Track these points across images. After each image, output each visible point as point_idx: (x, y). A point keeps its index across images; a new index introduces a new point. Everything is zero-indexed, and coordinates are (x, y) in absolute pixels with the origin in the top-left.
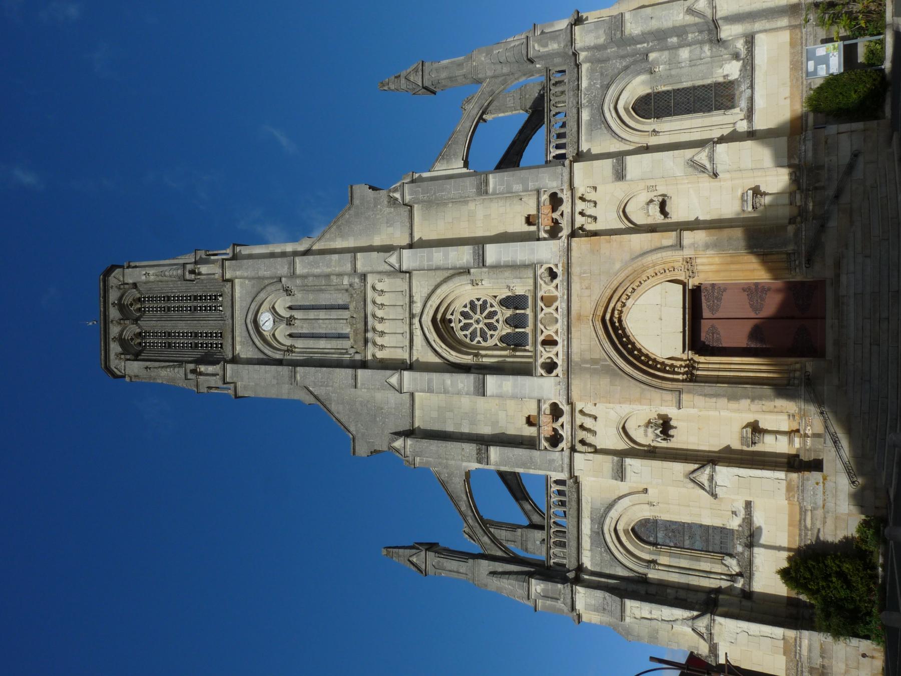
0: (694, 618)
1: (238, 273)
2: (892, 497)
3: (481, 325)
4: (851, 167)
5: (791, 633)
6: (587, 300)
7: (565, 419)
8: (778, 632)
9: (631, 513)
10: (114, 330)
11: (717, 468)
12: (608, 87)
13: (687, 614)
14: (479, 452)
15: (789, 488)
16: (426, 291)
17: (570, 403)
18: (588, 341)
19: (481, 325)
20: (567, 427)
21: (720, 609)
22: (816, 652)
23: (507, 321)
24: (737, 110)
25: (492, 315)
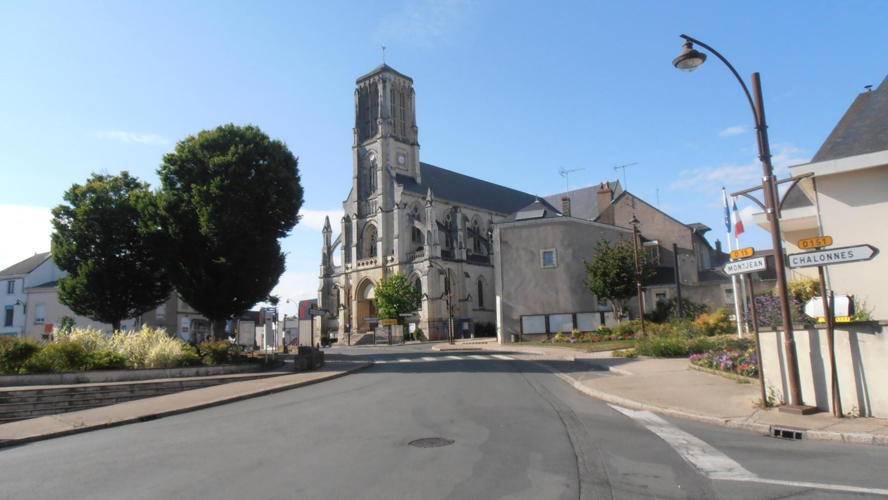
10: (367, 82)
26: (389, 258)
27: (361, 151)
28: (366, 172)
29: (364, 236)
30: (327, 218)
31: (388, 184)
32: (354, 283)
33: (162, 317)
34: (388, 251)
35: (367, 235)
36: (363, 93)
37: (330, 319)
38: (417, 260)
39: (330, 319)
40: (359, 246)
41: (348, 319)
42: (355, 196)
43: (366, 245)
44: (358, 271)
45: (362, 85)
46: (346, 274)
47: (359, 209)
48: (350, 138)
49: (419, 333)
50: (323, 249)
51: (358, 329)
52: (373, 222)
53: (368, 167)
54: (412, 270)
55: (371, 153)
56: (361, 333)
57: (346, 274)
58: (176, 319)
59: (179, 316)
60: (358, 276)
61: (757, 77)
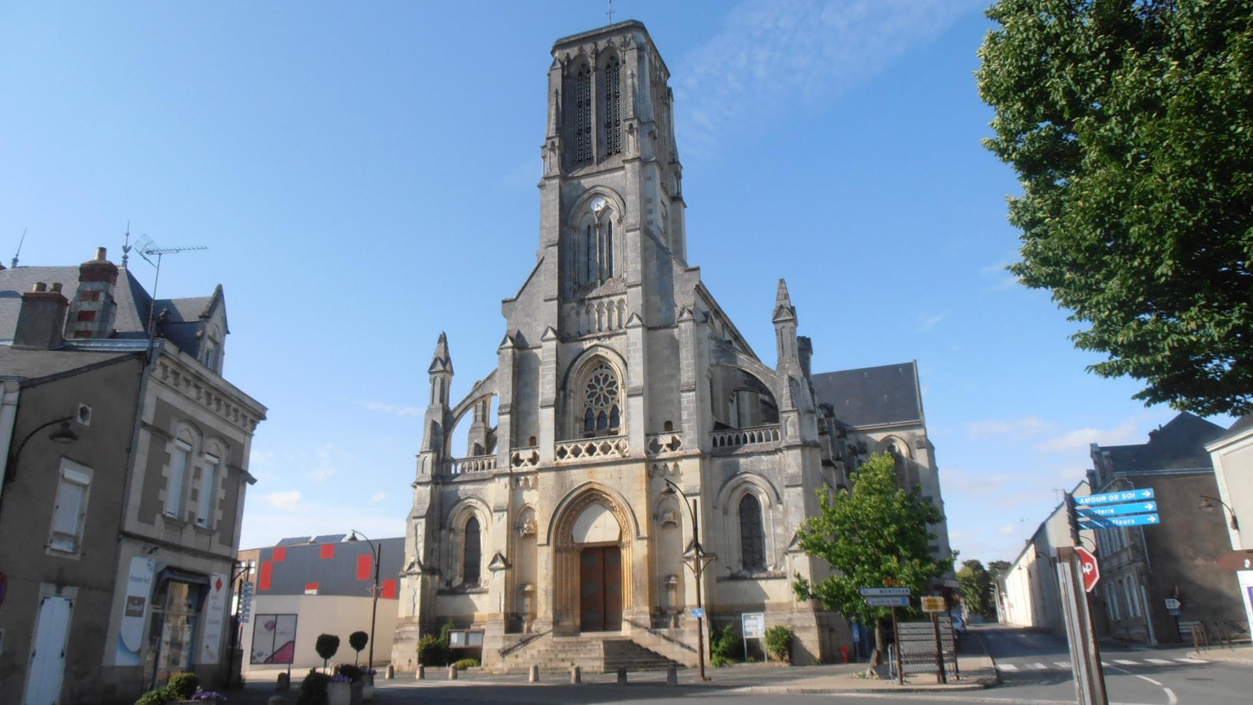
0: (419, 562)
1: (629, 175)
2: (765, 689)
3: (605, 389)
4: (682, 645)
5: (417, 619)
6: (603, 478)
7: (530, 467)
8: (417, 613)
9: (482, 516)
10: (588, 48)
11: (646, 542)
12: (761, 475)
13: (421, 559)
14: (505, 406)
15: (495, 615)
16: (617, 348)
17: (540, 470)
18: (579, 478)
19: (605, 389)
20: (525, 469)
21: (429, 578)
22: (408, 635)
23: (602, 412)
24: (741, 567)
25: (606, 399)
26: (665, 440)
27: (566, 189)
28: (579, 237)
29: (571, 385)
30: (443, 339)
31: (653, 264)
32: (541, 502)
33: (66, 546)
34: (660, 423)
35: (577, 382)
36: (574, 70)
37: (441, 592)
38: (749, 447)
39: (441, 592)
40: (560, 407)
41: (518, 592)
42: (549, 284)
43: (576, 406)
44: (558, 469)
45: (573, 52)
46: (515, 477)
47: (561, 319)
48: (531, 164)
49: (787, 644)
50: (430, 411)
51: (556, 623)
52: (602, 352)
53: (584, 227)
54: (733, 472)
55: (598, 195)
56: (564, 634)
57: (515, 477)
58: (116, 556)
59: (126, 548)
60: (561, 483)
61: (785, 314)
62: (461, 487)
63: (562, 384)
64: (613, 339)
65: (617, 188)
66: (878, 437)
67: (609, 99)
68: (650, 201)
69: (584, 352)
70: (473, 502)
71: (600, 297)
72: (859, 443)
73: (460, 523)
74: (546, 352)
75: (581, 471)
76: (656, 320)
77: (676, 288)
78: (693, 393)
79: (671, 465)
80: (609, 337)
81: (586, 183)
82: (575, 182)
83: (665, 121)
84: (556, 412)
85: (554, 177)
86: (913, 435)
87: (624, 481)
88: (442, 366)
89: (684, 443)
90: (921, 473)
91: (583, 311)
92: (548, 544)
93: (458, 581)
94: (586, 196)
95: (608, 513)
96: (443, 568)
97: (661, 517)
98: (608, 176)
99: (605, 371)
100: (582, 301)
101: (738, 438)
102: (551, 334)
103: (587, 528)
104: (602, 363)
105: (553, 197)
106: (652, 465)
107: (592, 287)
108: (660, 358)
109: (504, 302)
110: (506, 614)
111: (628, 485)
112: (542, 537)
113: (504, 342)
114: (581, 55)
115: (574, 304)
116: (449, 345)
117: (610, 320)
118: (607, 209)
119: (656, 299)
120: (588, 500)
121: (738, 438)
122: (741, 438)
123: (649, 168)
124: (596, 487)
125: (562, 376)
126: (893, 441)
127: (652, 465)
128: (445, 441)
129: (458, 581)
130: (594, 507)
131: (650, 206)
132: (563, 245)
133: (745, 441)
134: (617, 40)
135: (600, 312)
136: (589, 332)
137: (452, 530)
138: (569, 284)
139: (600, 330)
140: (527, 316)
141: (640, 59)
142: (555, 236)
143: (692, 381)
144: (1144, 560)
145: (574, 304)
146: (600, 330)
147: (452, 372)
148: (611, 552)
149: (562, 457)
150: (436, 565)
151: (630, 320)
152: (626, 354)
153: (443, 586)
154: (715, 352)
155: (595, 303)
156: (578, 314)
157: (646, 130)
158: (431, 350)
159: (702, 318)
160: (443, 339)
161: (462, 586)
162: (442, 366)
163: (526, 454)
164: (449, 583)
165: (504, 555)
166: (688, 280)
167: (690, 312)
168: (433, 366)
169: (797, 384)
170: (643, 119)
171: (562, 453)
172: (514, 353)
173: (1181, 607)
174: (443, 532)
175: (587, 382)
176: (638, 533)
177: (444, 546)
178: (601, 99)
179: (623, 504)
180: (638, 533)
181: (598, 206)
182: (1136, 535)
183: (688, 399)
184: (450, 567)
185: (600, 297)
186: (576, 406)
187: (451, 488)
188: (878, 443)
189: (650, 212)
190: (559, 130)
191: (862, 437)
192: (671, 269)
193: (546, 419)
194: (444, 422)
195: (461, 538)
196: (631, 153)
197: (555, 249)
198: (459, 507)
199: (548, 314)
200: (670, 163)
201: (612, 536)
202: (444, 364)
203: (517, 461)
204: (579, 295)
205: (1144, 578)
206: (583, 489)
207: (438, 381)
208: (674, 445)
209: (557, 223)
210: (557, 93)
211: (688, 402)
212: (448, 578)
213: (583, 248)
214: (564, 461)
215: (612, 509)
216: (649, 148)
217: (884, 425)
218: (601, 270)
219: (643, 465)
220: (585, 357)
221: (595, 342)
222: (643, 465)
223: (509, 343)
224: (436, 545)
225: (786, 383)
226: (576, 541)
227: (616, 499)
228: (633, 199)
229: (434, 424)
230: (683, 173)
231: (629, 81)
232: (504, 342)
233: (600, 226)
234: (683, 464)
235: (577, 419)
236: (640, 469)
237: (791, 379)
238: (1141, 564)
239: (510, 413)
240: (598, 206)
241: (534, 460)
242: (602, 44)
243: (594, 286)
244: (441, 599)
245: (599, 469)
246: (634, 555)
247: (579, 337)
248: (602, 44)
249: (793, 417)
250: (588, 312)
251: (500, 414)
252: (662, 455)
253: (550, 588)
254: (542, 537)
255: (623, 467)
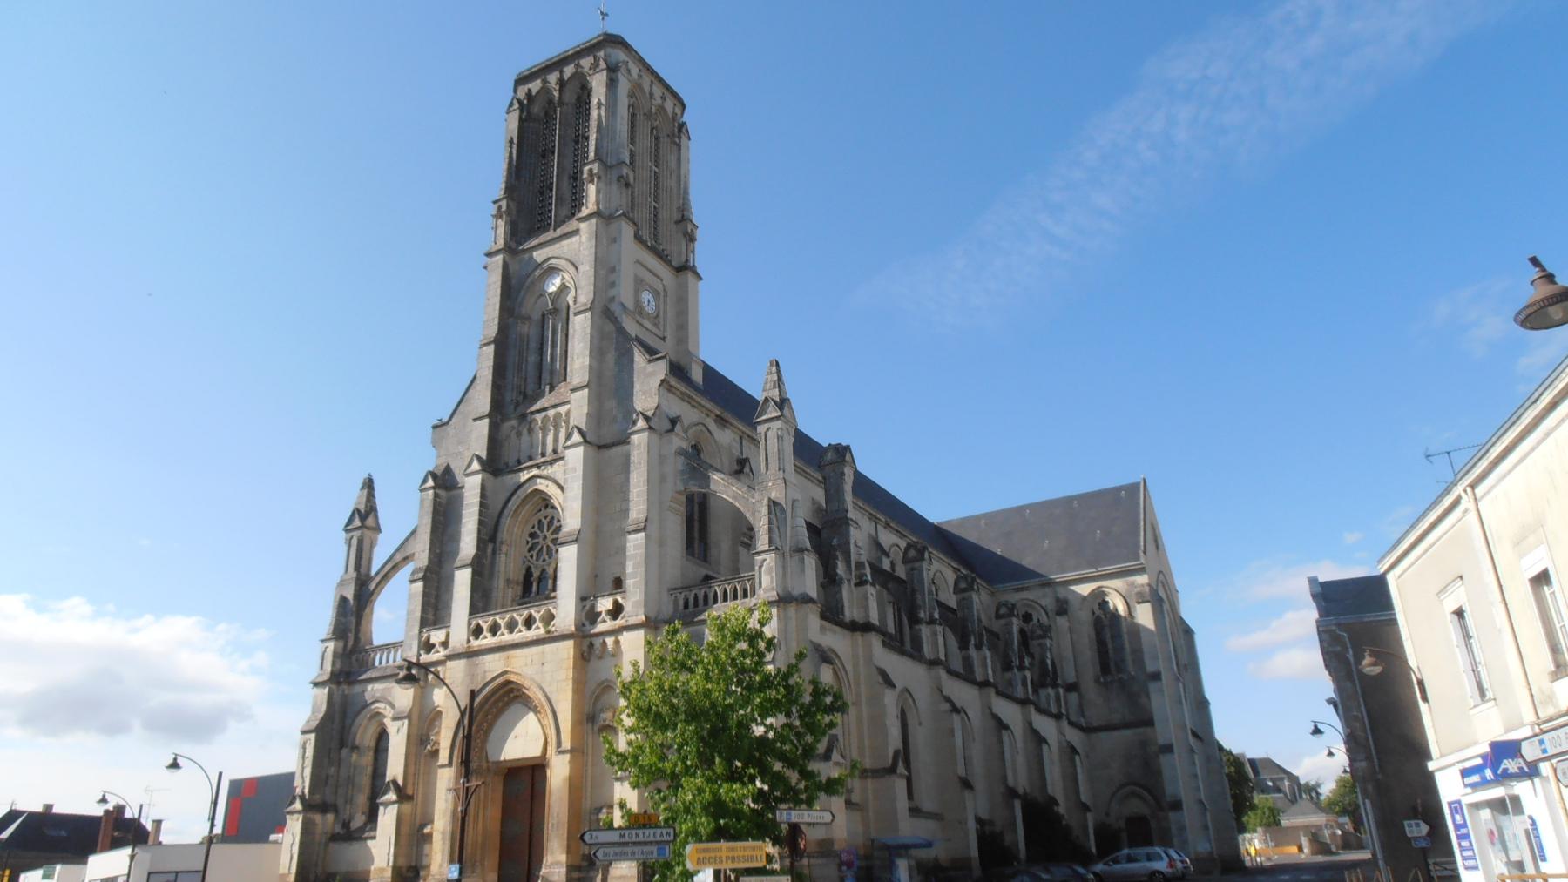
6: (526, 666)
10: (553, 78)
11: (567, 757)
18: (493, 665)
27: (513, 268)
28: (527, 330)
29: (503, 535)
30: (369, 485)
31: (611, 357)
34: (602, 578)
35: (514, 531)
36: (536, 109)
37: (335, 838)
39: (335, 838)
40: (482, 569)
42: (482, 400)
43: (509, 565)
44: (470, 654)
45: (535, 86)
47: (494, 442)
50: (342, 584)
52: (542, 485)
53: (536, 316)
55: (553, 270)
62: (370, 687)
63: (489, 535)
64: (556, 466)
65: (572, 259)
66: (1084, 589)
67: (577, 142)
68: (613, 270)
69: (520, 486)
70: (380, 706)
71: (545, 409)
72: (1058, 600)
73: (366, 737)
74: (472, 485)
75: (497, 656)
76: (608, 434)
77: (637, 387)
78: (642, 534)
79: (610, 641)
80: (551, 463)
81: (539, 255)
82: (526, 256)
83: (673, 165)
84: (474, 574)
85: (497, 252)
86: (1132, 585)
87: (547, 667)
88: (365, 518)
89: (628, 608)
90: (1145, 639)
91: (525, 431)
92: (450, 764)
93: (358, 821)
94: (537, 273)
95: (531, 715)
96: (340, 802)
97: (592, 717)
98: (565, 243)
99: (549, 510)
100: (523, 417)
101: (706, 596)
102: (476, 466)
103: (504, 740)
104: (545, 502)
105: (495, 279)
106: (586, 642)
107: (539, 395)
108: (604, 490)
109: (435, 427)
110: (394, 868)
111: (548, 671)
112: (443, 757)
113: (425, 481)
114: (545, 89)
115: (514, 422)
116: (377, 493)
117: (556, 440)
118: (563, 288)
119: (611, 404)
120: (506, 698)
121: (706, 596)
122: (711, 596)
123: (614, 226)
124: (513, 678)
125: (491, 523)
126: (1104, 594)
127: (586, 642)
128: (358, 624)
129: (358, 821)
130: (516, 708)
131: (612, 277)
132: (503, 343)
133: (715, 602)
134: (586, 62)
135: (544, 429)
136: (531, 459)
137: (355, 748)
138: (510, 396)
139: (543, 455)
140: (460, 443)
141: (612, 84)
142: (493, 330)
143: (643, 517)
144: (1369, 758)
145: (514, 422)
146: (543, 455)
147: (378, 529)
148: (534, 771)
149: (477, 638)
150: (330, 799)
151: (569, 436)
152: (565, 483)
153: (338, 829)
154: (683, 472)
155: (539, 417)
156: (519, 434)
157: (614, 174)
158: (353, 498)
159: (668, 426)
160: (369, 485)
161: (362, 829)
162: (365, 518)
163: (437, 636)
164: (346, 825)
165: (400, 782)
166: (652, 374)
167: (647, 419)
168: (350, 521)
169: (783, 511)
170: (611, 161)
171: (477, 632)
172: (436, 495)
173: (1429, 834)
174: (345, 751)
175: (528, 530)
176: (559, 744)
177: (343, 772)
178: (578, 145)
179: (545, 703)
180: (559, 744)
181: (553, 286)
182: (1356, 718)
183: (635, 544)
184: (349, 800)
185: (545, 409)
186: (509, 565)
187: (357, 688)
188: (1084, 598)
189: (613, 285)
190: (510, 190)
191: (1061, 592)
192: (632, 361)
193: (462, 580)
194: (357, 596)
195: (368, 759)
196: (589, 207)
197: (491, 348)
198: (366, 714)
199: (477, 437)
200: (677, 222)
201: (534, 751)
202: (363, 518)
203: (428, 647)
204: (520, 410)
205: (1370, 788)
206: (498, 681)
207: (354, 542)
208: (616, 611)
209: (497, 313)
210: (511, 142)
211: (636, 547)
212: (346, 816)
213: (533, 345)
214: (476, 644)
215: (535, 710)
216: (619, 199)
217: (1091, 572)
218: (552, 372)
219: (570, 643)
220: (521, 493)
221: (535, 472)
222: (570, 643)
223: (431, 483)
224: (332, 770)
225: (765, 510)
226: (491, 759)
227: (534, 693)
228: (587, 268)
229: (343, 600)
230: (699, 234)
231: (594, 113)
232: (425, 481)
233: (555, 311)
234: (625, 638)
235: (508, 582)
236: (567, 649)
237: (773, 504)
238: (1364, 764)
239: (424, 578)
240: (553, 286)
241: (445, 644)
242: (569, 70)
243: (540, 395)
244: (334, 846)
245: (518, 652)
246: (559, 772)
247: (517, 467)
248: (569, 70)
249: (770, 559)
250: (530, 431)
251: (412, 581)
252: (600, 628)
253: (449, 829)
254: (443, 757)
255: (548, 648)
